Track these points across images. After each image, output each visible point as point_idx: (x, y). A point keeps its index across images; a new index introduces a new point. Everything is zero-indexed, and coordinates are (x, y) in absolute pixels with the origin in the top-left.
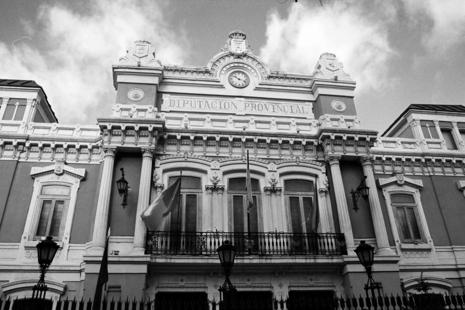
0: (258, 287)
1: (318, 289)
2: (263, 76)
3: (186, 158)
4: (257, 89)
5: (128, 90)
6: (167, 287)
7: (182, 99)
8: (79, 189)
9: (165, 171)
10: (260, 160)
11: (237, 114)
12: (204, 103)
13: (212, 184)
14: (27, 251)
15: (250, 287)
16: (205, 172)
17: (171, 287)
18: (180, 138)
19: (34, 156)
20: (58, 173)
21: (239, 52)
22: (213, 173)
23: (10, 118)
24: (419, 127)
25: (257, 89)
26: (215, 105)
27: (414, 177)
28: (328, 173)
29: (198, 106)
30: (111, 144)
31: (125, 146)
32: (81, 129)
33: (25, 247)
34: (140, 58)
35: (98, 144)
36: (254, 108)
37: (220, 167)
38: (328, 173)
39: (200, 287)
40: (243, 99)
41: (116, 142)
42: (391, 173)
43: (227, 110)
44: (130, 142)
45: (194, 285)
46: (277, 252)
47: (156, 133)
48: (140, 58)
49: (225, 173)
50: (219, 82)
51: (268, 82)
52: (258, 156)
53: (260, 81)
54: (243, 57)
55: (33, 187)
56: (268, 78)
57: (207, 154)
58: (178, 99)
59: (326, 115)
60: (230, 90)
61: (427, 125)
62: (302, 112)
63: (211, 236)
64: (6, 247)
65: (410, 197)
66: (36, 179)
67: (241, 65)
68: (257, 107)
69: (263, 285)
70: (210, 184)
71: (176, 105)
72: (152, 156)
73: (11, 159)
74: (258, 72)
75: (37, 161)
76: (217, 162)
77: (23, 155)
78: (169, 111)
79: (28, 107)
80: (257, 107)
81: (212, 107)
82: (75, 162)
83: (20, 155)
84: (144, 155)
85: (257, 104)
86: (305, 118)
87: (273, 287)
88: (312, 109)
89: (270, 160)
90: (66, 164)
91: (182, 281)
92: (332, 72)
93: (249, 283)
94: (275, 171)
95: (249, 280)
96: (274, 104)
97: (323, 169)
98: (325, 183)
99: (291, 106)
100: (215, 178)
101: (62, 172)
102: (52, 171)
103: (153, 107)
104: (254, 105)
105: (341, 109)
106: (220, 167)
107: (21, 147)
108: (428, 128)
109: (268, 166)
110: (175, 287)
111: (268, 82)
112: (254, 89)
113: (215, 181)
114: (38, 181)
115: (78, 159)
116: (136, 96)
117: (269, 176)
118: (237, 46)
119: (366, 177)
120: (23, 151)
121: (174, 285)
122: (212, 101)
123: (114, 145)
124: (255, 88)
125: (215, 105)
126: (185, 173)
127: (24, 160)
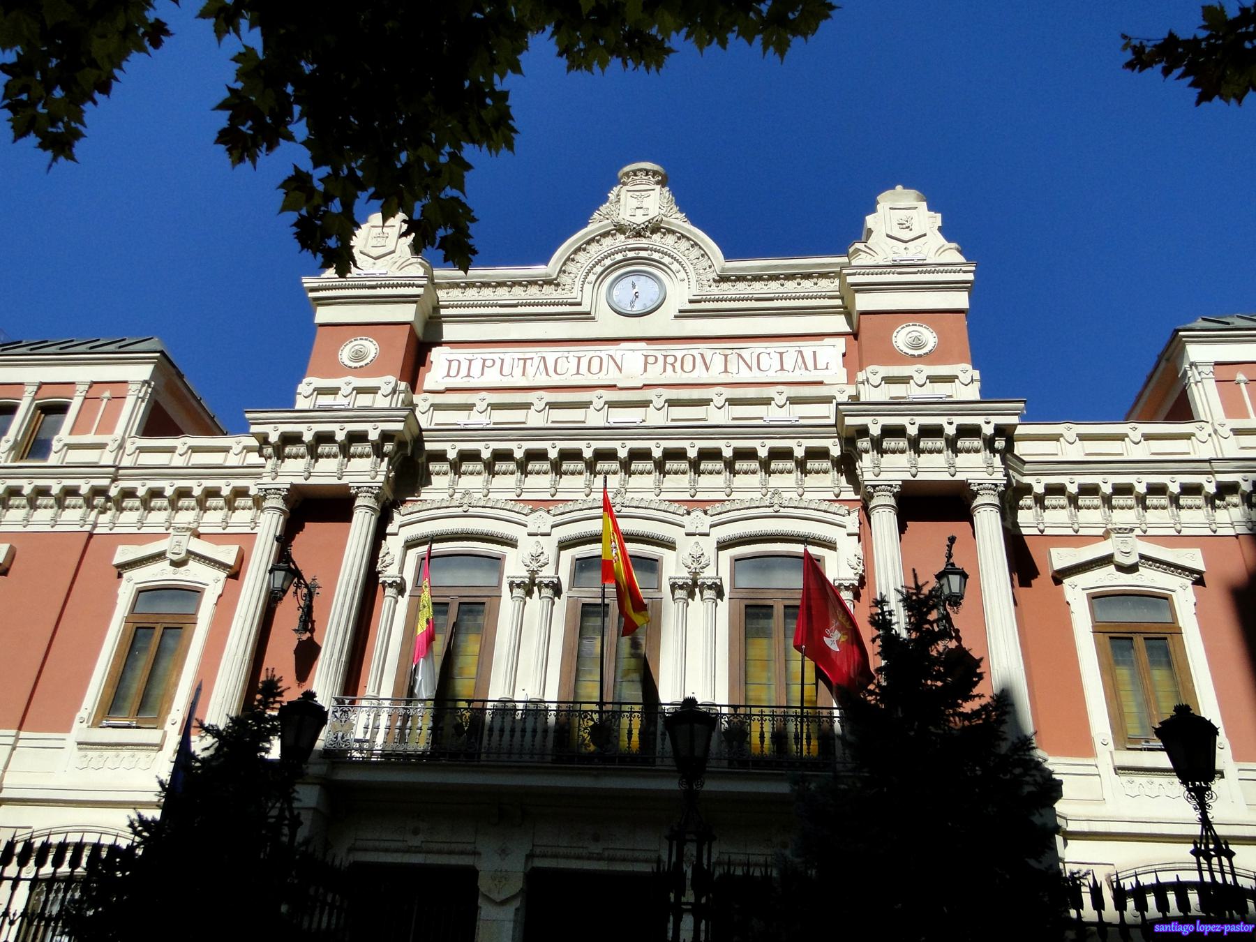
0: (624, 860)
1: (563, 864)
2: (703, 277)
3: (776, 507)
4: (683, 314)
5: (342, 342)
6: (376, 850)
7: (479, 356)
8: (220, 596)
9: (410, 544)
10: (824, 506)
11: (619, 385)
12: (536, 360)
13: (527, 574)
14: (83, 753)
15: (600, 858)
16: (670, 545)
17: (386, 850)
18: (556, 455)
19: (129, 520)
20: (175, 558)
21: (640, 219)
22: (533, 547)
23: (87, 432)
24: (1211, 386)
25: (683, 314)
26: (567, 367)
27: (1178, 540)
28: (864, 536)
29: (518, 371)
30: (278, 480)
31: (312, 481)
32: (245, 448)
33: (79, 744)
34: (376, 259)
35: (79, 487)
36: (669, 368)
37: (711, 526)
38: (864, 536)
39: (462, 853)
40: (642, 345)
41: (294, 471)
42: (1100, 532)
43: (596, 377)
44: (934, 467)
45: (446, 847)
46: (510, 753)
47: (388, 447)
48: (376, 259)
49: (564, 545)
50: (579, 304)
51: (716, 290)
52: (664, 496)
53: (694, 292)
54: (652, 233)
55: (117, 596)
56: (715, 281)
57: (524, 496)
58: (470, 357)
59: (870, 368)
60: (607, 324)
61: (1241, 377)
62: (810, 364)
63: (762, 715)
64: (34, 743)
65: (1162, 599)
66: (126, 575)
67: (643, 254)
68: (678, 365)
69: (637, 854)
70: (684, 575)
71: (464, 371)
72: (997, 503)
73: (77, 528)
74: (690, 269)
75: (135, 530)
76: (545, 514)
77: (105, 518)
78: (442, 388)
79: (130, 401)
80: (678, 365)
81: (555, 371)
82: (220, 530)
83: (97, 518)
84: (358, 502)
85: (679, 354)
86: (821, 383)
87: (479, 854)
88: (844, 355)
89: (693, 504)
90: (198, 536)
91: (416, 832)
92: (904, 245)
93: (596, 848)
94: (708, 535)
95: (596, 839)
96: (729, 352)
97: (852, 521)
98: (854, 562)
99: (781, 354)
100: (697, 559)
101: (183, 555)
102: (160, 556)
103: (969, 367)
104: (671, 360)
105: (924, 346)
106: (711, 526)
107: (99, 501)
108: (1242, 385)
109: (685, 520)
110: (397, 851)
111: (716, 290)
112: (676, 317)
113: (534, 566)
114: (130, 580)
115: (226, 524)
116: (358, 356)
117: (687, 547)
118: (635, 203)
119: (278, 539)
120: (104, 511)
121: (393, 845)
122: (559, 354)
123: (285, 481)
124: (677, 313)
125: (567, 367)
126: (438, 548)
127: (106, 531)
